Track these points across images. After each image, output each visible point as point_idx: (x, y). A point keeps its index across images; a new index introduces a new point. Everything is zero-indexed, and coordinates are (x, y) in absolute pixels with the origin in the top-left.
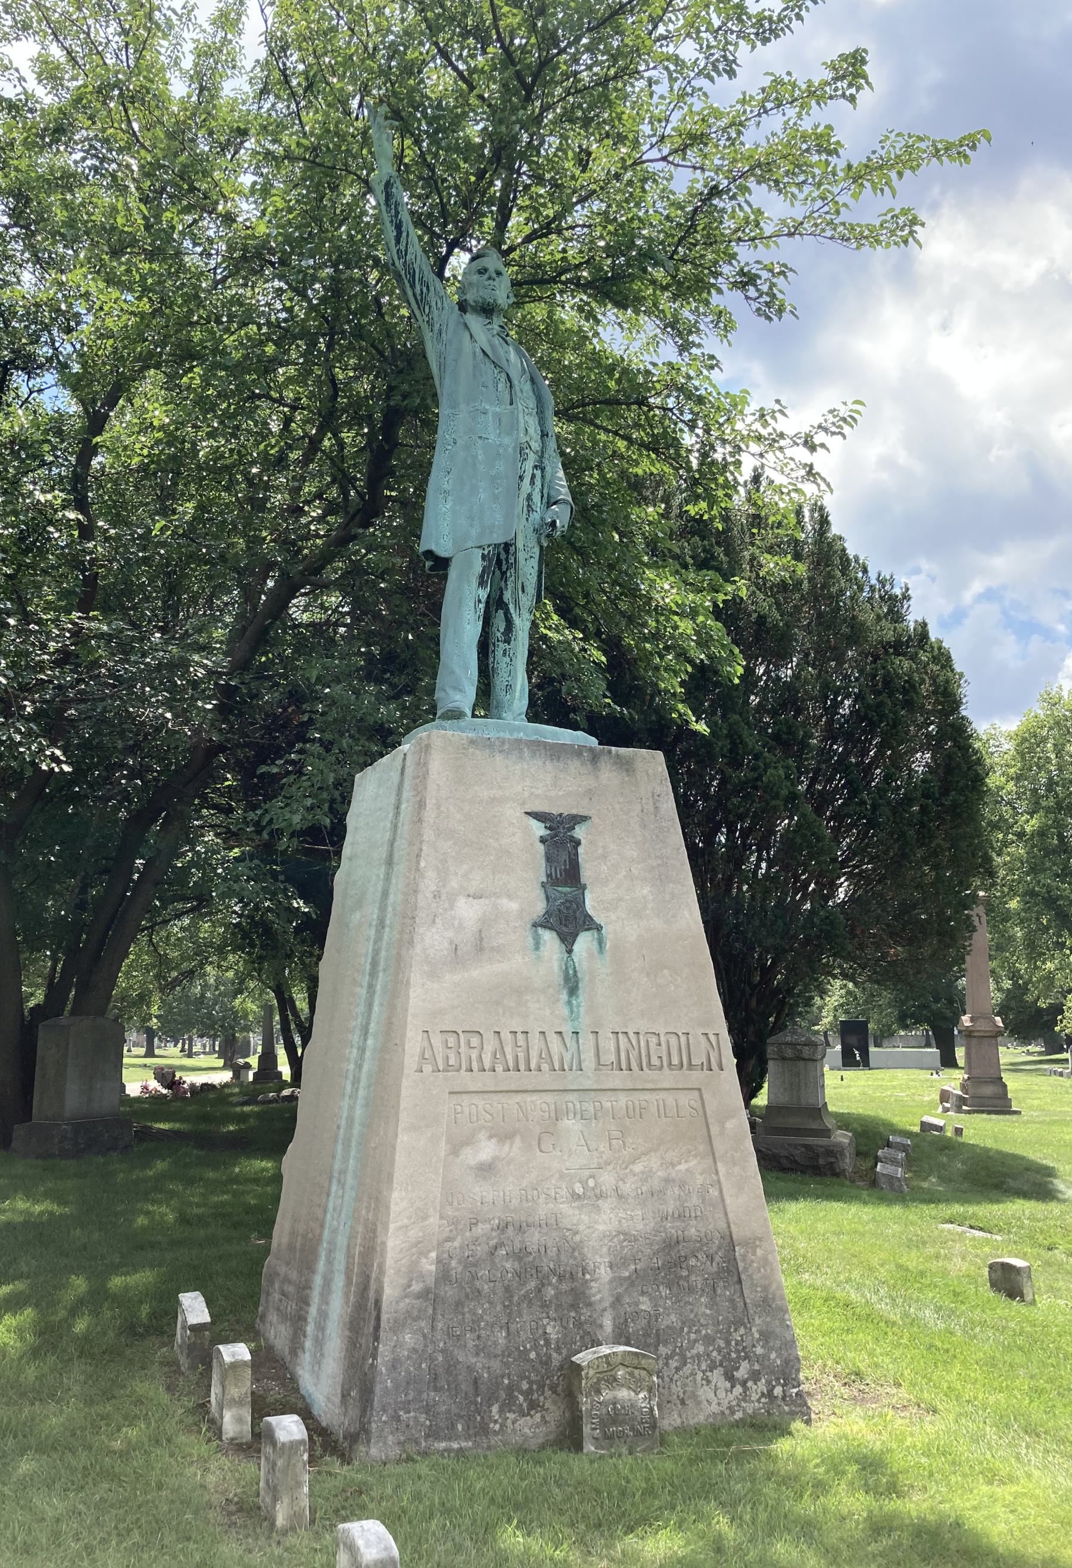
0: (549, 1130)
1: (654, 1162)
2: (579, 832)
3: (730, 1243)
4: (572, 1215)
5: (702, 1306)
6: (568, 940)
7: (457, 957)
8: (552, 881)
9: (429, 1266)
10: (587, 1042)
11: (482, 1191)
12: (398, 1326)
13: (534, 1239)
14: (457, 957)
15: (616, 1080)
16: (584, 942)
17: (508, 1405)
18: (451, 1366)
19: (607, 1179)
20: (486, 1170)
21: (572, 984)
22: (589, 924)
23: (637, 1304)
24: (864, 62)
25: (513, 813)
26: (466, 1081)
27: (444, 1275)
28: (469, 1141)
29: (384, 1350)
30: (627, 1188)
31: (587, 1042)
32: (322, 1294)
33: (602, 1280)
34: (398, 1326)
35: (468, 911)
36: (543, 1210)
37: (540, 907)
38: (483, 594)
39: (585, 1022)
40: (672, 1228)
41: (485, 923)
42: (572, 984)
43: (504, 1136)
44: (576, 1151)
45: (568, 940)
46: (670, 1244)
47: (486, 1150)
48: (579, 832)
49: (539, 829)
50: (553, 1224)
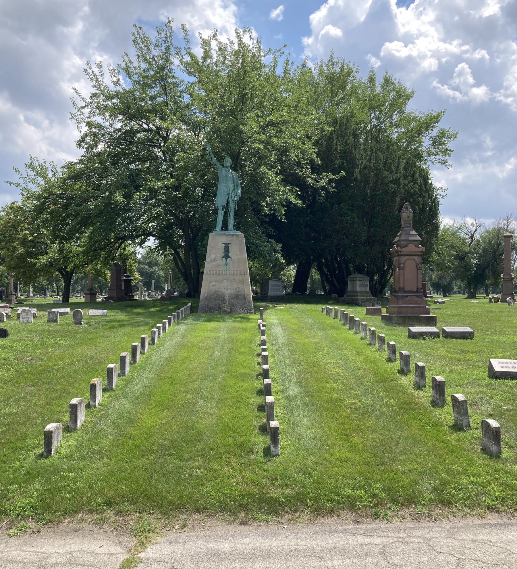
0: (222, 281)
1: (236, 285)
2: (229, 245)
3: (245, 295)
4: (224, 290)
5: (240, 302)
6: (226, 259)
7: (211, 261)
8: (225, 252)
9: (206, 295)
10: (228, 272)
11: (213, 288)
12: (202, 301)
13: (219, 293)
14: (211, 261)
15: (231, 276)
16: (229, 259)
17: (214, 310)
18: (208, 305)
19: (229, 287)
20: (214, 285)
21: (226, 264)
22: (229, 257)
23: (336, 159)
24: (409, 99)
25: (220, 243)
26: (212, 276)
27: (208, 296)
28: (212, 282)
29: (200, 304)
30: (232, 288)
31: (228, 272)
32: (163, 330)
33: (227, 297)
34: (202, 301)
35: (213, 256)
36: (220, 290)
37: (223, 255)
38: (223, 212)
39: (228, 269)
40: (237, 293)
41: (215, 257)
42: (226, 264)
43: (216, 282)
44: (225, 283)
45: (226, 259)
46: (236, 295)
47: (214, 283)
48: (229, 245)
49: (224, 245)
50: (222, 292)
